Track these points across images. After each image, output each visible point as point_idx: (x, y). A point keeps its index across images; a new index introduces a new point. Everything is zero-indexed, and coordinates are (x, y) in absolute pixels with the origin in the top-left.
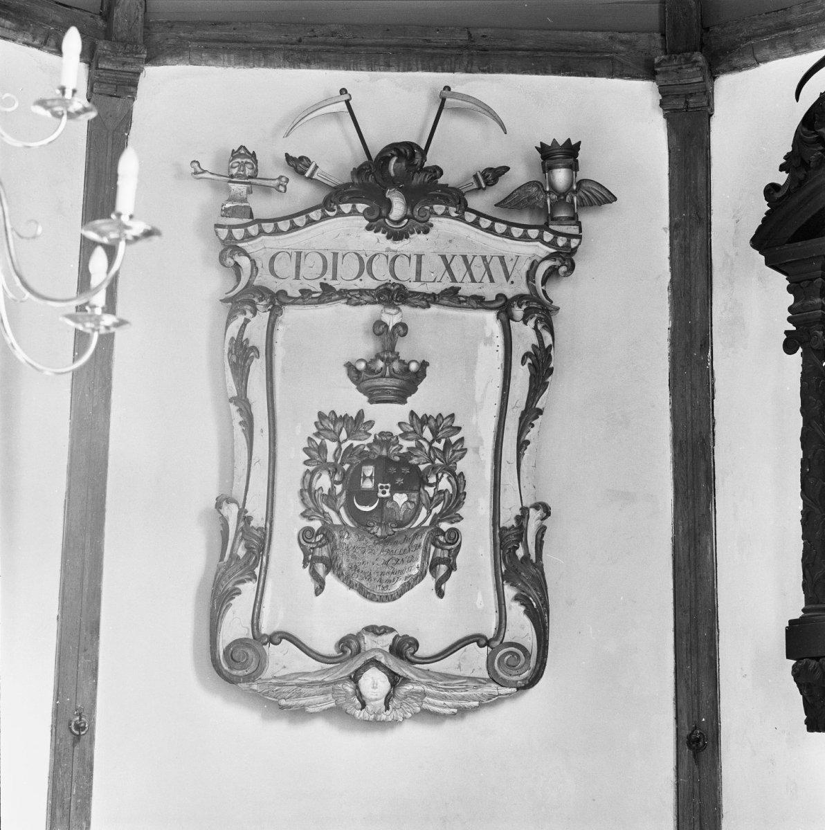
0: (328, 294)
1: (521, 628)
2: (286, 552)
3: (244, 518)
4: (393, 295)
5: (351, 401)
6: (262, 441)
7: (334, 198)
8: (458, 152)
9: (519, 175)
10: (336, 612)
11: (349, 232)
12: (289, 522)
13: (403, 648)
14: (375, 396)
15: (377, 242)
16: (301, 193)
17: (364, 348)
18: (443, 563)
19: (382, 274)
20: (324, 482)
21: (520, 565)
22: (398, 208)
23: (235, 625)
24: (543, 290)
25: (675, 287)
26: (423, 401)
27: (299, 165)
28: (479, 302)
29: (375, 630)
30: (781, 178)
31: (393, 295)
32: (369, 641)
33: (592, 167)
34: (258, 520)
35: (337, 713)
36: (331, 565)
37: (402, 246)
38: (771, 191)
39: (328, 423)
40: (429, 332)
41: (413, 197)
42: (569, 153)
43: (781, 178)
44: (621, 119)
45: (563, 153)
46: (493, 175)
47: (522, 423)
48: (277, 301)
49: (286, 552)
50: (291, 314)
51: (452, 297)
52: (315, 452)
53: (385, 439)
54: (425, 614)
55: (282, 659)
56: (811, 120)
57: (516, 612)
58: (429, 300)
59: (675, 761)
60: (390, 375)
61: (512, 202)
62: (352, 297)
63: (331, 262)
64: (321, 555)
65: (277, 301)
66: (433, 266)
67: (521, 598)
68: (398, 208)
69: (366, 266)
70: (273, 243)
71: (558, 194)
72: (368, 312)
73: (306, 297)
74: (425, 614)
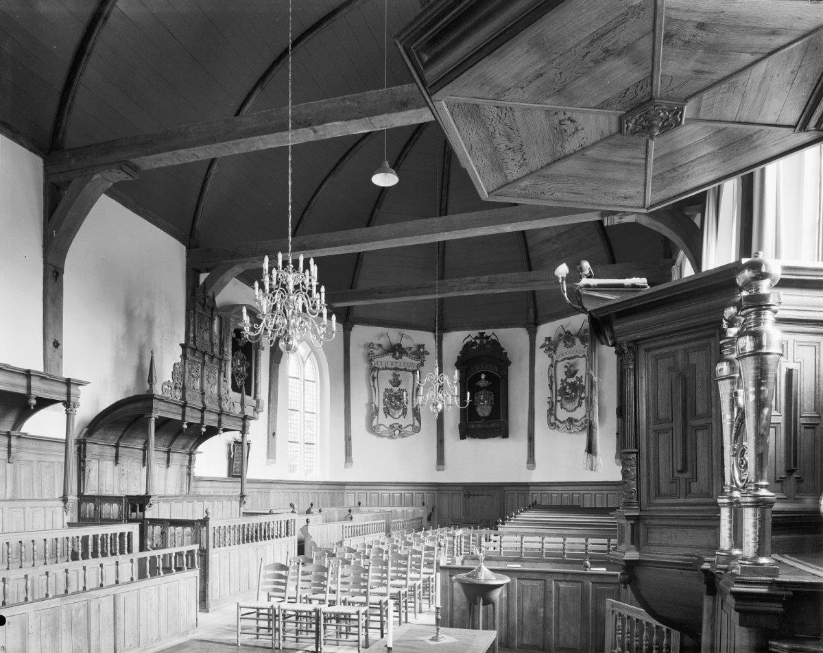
0: (386, 368)
1: (417, 424)
2: (381, 412)
3: (375, 405)
4: (396, 369)
5: (390, 386)
6: (377, 393)
7: (387, 352)
8: (405, 344)
9: (413, 349)
10: (389, 421)
11: (389, 358)
12: (382, 407)
13: (400, 426)
14: (394, 386)
15: (394, 360)
16: (380, 351)
17: (391, 378)
18: (405, 413)
19: (395, 366)
20: (386, 400)
21: (416, 413)
22: (398, 355)
23: (375, 423)
24: (796, 467)
25: (724, 467)
26: (401, 387)
27: (380, 345)
28: (410, 371)
29: (396, 424)
30: (460, 355)
31: (396, 369)
32: (395, 426)
33: (426, 348)
34: (377, 405)
35: (391, 437)
36: (389, 414)
37: (398, 361)
38: (458, 357)
39: (386, 390)
40: (403, 376)
41: (400, 353)
42: (423, 346)
43: (460, 355)
44: (426, 339)
45: (421, 346)
46: (410, 348)
47: (714, 392)
48: (379, 369)
49: (381, 412)
50: (380, 371)
51: (405, 370)
52: (385, 395)
53: (396, 393)
54: (403, 422)
55: (382, 428)
56: (465, 346)
57: (416, 421)
58: (401, 370)
59: (803, 143)
60: (396, 383)
61: (413, 353)
62: (390, 369)
63: (387, 363)
64: (387, 412)
65: (379, 369)
66: (402, 364)
67: (417, 419)
68: (398, 355)
69: (392, 364)
70: (377, 359)
71: (420, 353)
72: (392, 372)
73: (383, 369)
74: (403, 422)
